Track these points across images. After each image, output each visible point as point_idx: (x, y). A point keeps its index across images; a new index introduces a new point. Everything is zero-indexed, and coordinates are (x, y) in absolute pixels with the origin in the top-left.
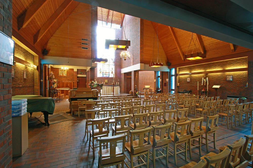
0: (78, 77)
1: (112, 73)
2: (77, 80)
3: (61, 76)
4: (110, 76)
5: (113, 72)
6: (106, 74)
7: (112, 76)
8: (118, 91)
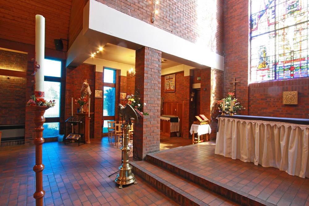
3: (168, 91)
7: (104, 87)
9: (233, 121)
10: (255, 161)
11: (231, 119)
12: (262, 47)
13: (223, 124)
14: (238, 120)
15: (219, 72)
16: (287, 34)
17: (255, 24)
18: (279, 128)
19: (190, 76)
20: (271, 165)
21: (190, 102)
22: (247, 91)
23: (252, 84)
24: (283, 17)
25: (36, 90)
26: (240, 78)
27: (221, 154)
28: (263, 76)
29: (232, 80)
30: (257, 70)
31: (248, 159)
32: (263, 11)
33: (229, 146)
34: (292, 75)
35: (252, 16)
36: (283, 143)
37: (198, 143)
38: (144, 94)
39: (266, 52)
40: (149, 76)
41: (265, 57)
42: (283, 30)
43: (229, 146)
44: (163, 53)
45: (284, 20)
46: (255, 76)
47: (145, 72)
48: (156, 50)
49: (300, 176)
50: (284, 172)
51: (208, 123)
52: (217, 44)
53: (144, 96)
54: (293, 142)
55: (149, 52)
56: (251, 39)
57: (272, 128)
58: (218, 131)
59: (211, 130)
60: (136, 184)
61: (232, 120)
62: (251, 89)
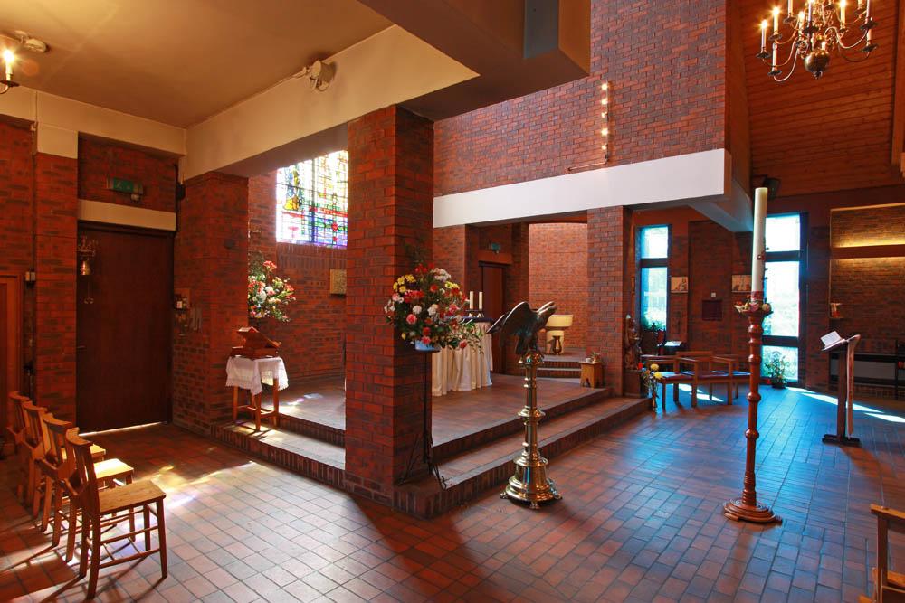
0: (86, 227)
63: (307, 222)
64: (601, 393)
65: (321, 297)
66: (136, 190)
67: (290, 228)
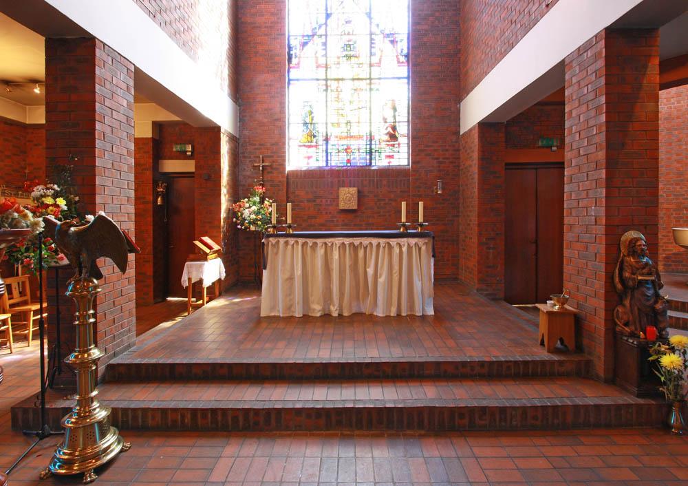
1: (393, 137)
2: (156, 195)
4: (380, 162)
5: (403, 129)
6: (348, 150)
7: (401, 157)
8: (417, 284)
9: (295, 245)
10: (332, 308)
11: (292, 241)
12: (306, 104)
13: (275, 251)
14: (303, 240)
15: (233, 139)
16: (341, 91)
17: (296, 57)
18: (365, 248)
19: (153, 139)
20: (354, 311)
21: (153, 207)
22: (286, 185)
23: (292, 171)
24: (336, 60)
25: (160, 171)
26: (272, 156)
27: (273, 314)
28: (309, 158)
29: (257, 160)
30: (300, 146)
31: (324, 309)
32: (308, 36)
33: (289, 293)
34: (349, 161)
35: (291, 37)
36: (370, 271)
37: (203, 304)
38: (97, 183)
39: (313, 115)
40: (108, 130)
41: (311, 124)
42: (336, 82)
43: (289, 293)
44: (136, 68)
45: (338, 66)
46: (298, 159)
47: (97, 117)
48: (123, 59)
49: (392, 315)
50: (371, 315)
51: (219, 256)
52: (229, 75)
53: (97, 191)
54: (382, 267)
55: (105, 57)
56: (289, 84)
57: (355, 248)
58: (265, 268)
59: (224, 270)
60: (129, 448)
61: (293, 242)
62: (291, 180)
63: (321, 151)
64: (552, 363)
65: (330, 213)
66: (555, 144)
67: (305, 158)
